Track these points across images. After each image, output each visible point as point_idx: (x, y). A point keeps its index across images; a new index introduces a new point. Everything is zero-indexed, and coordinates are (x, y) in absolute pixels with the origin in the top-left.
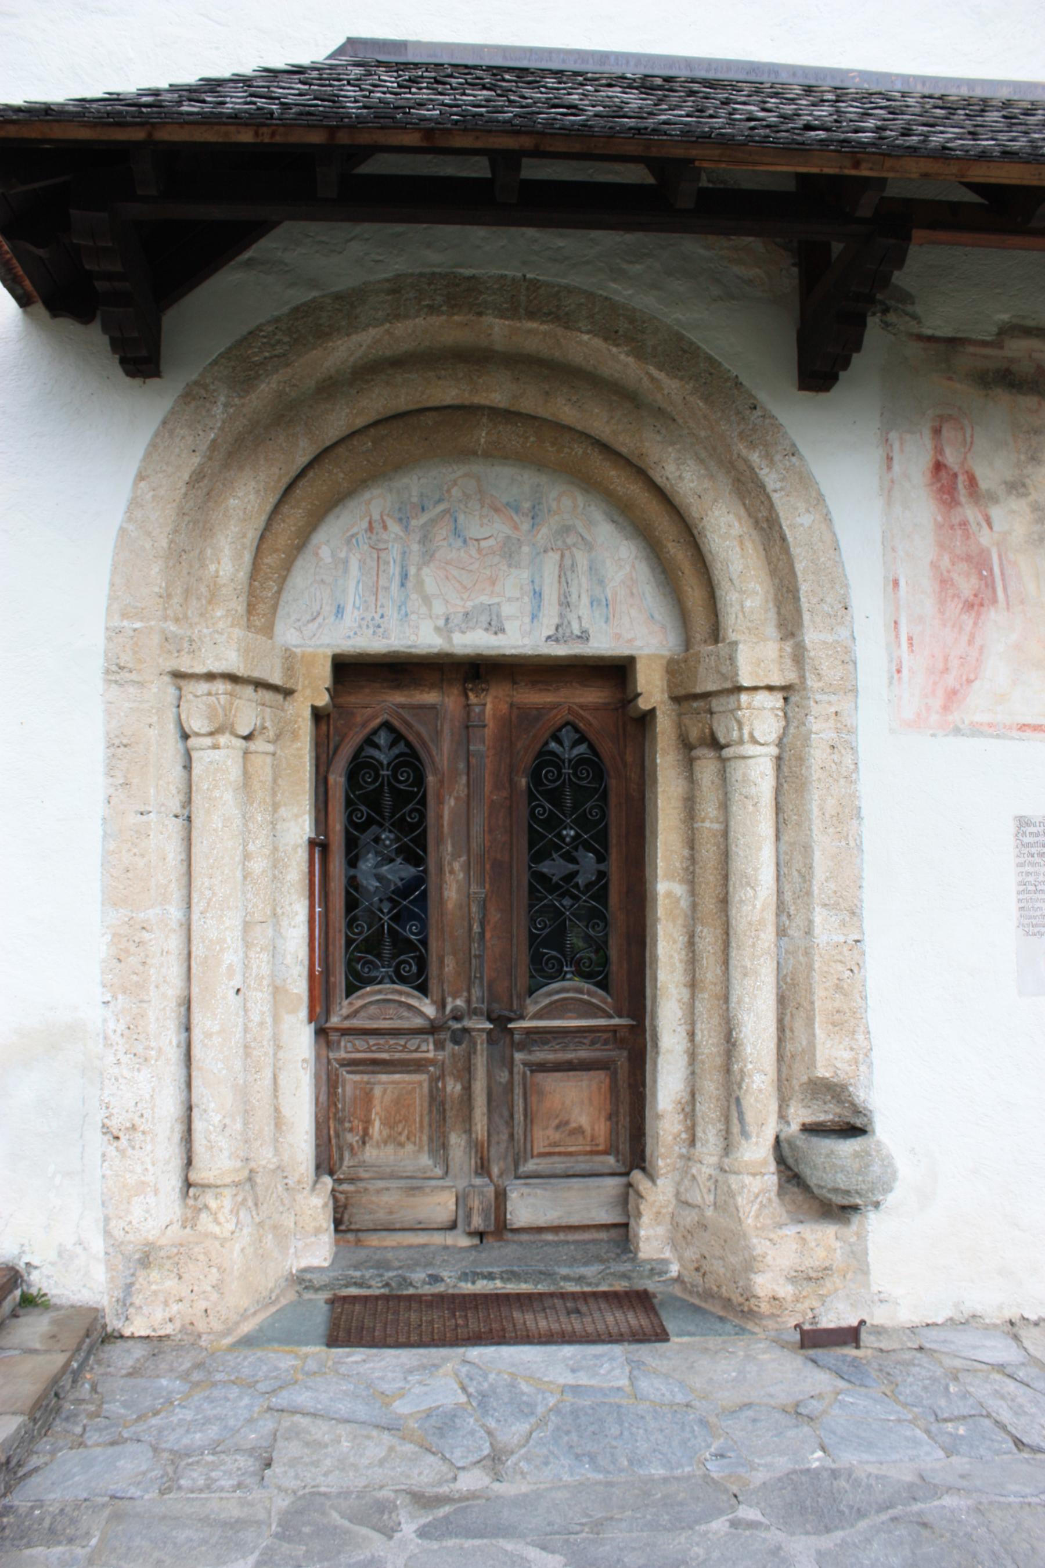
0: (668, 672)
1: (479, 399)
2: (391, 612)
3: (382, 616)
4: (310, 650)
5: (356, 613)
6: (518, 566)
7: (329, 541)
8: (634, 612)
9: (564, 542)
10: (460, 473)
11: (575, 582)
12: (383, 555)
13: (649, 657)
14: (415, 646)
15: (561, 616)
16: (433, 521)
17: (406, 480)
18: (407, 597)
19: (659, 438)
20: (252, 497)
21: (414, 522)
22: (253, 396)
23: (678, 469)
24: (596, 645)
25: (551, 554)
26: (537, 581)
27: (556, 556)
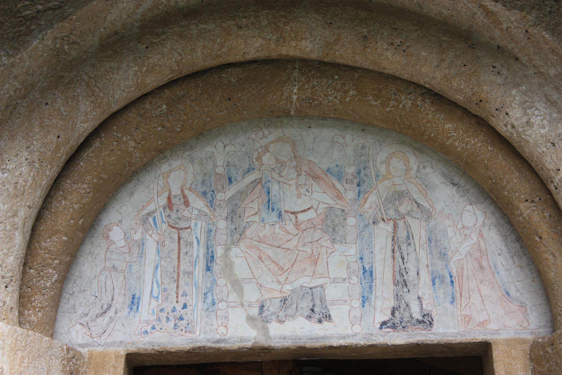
0: (531, 359)
1: (288, 50)
2: (195, 301)
3: (185, 306)
4: (100, 349)
5: (154, 303)
6: (343, 241)
7: (122, 223)
8: (485, 290)
9: (397, 211)
10: (271, 138)
11: (412, 256)
12: (184, 234)
13: (508, 342)
14: (224, 341)
15: (397, 297)
16: (242, 194)
17: (209, 149)
18: (214, 283)
19: (499, 80)
20: (25, 169)
21: (220, 196)
22: (24, 54)
23: (525, 114)
24: (441, 331)
25: (381, 225)
26: (366, 258)
27: (389, 228)
